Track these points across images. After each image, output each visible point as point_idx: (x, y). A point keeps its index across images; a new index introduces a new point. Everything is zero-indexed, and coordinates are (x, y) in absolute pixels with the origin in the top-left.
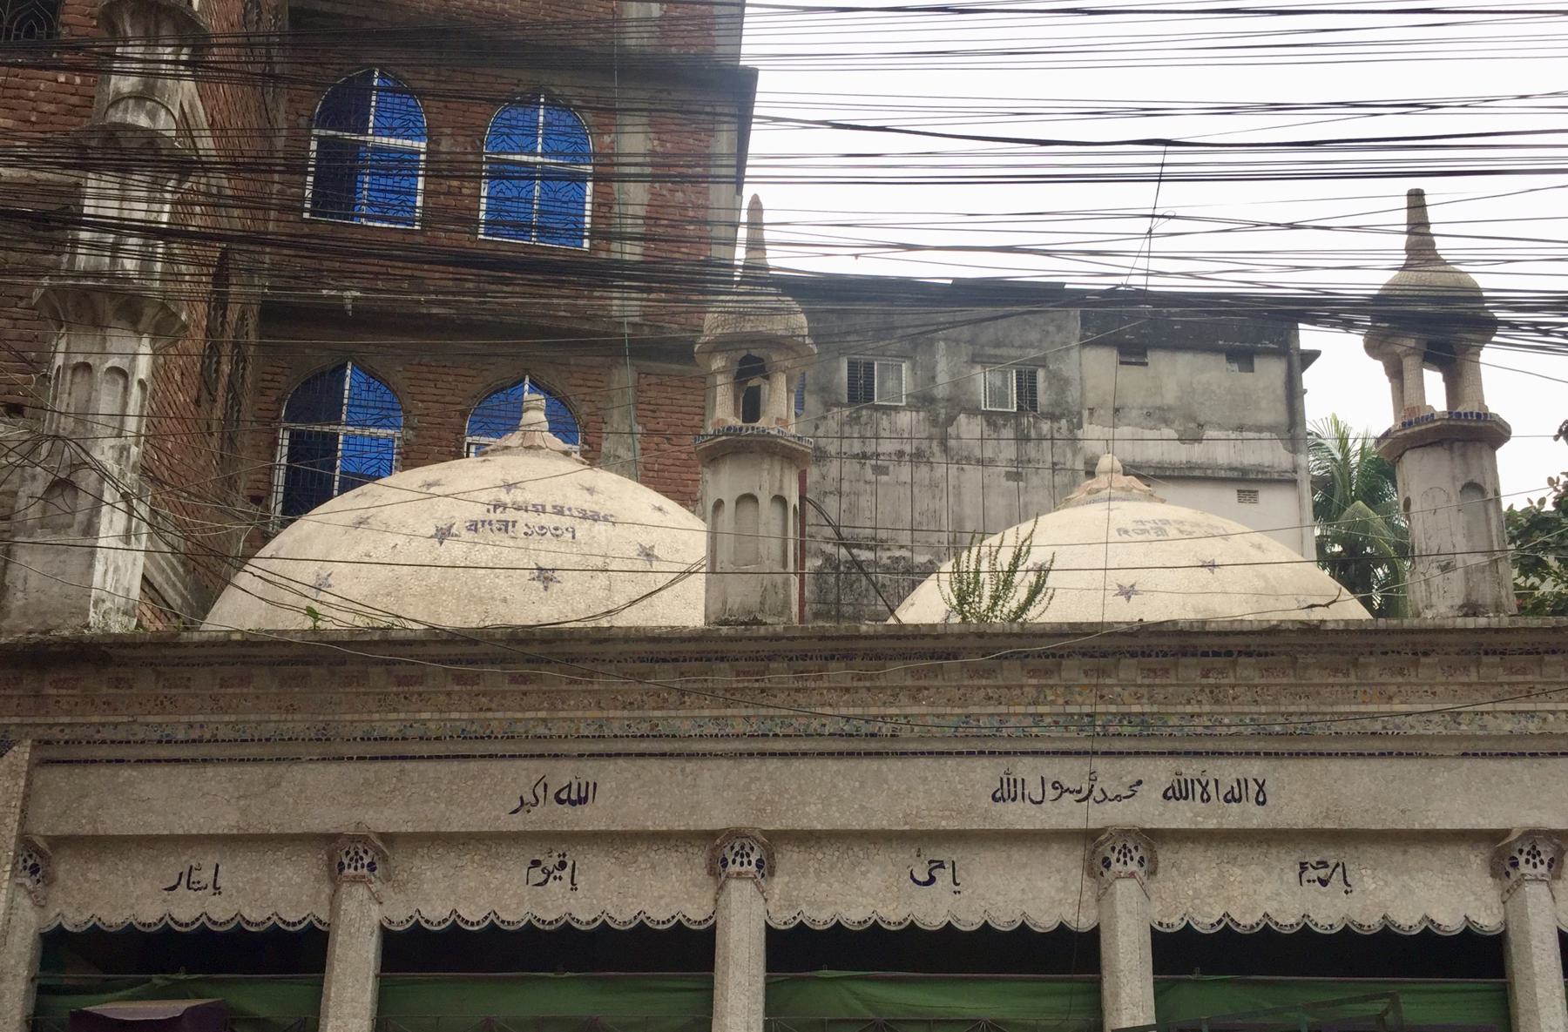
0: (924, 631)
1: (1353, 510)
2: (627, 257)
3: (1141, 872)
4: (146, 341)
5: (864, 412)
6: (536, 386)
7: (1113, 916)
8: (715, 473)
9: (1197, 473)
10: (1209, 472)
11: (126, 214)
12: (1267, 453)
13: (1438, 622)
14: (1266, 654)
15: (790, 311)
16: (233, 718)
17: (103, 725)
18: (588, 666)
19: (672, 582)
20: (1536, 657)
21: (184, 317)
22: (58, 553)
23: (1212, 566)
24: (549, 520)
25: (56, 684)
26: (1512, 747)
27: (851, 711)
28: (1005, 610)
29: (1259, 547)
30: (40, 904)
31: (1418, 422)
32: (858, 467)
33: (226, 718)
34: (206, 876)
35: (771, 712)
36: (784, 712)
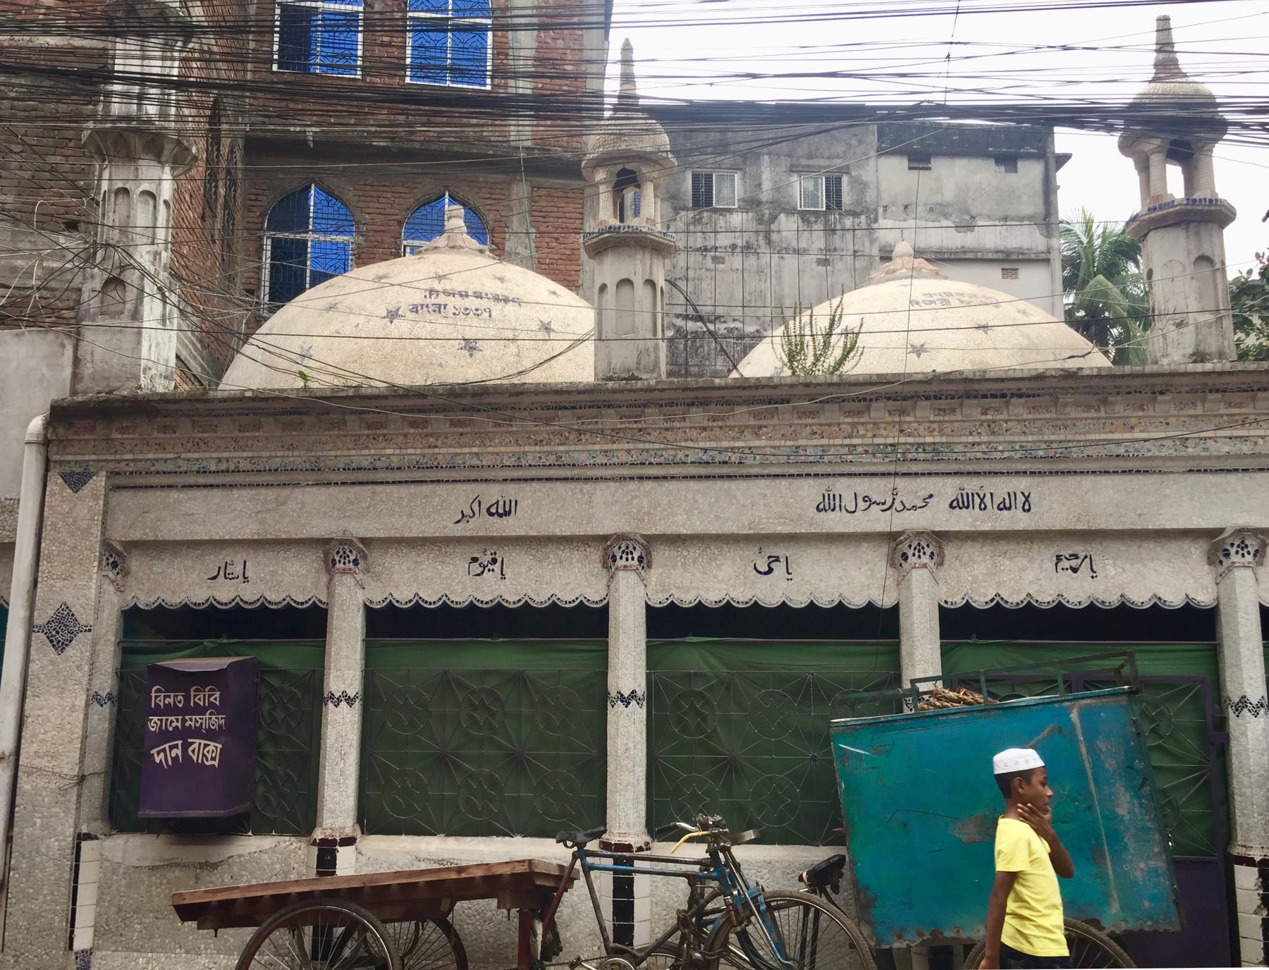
0: (764, 382)
1: (1097, 283)
2: (521, 91)
3: (931, 564)
4: (167, 169)
5: (705, 214)
6: (454, 199)
7: (910, 598)
8: (600, 262)
9: (969, 256)
10: (979, 255)
11: (146, 70)
12: (1026, 238)
13: (1173, 368)
14: (1034, 396)
15: (655, 132)
16: (250, 454)
17: (157, 460)
18: (509, 412)
19: (570, 348)
20: (1250, 394)
21: (194, 150)
22: (114, 334)
23: (985, 327)
24: (471, 303)
25: (122, 430)
26: (1229, 464)
27: (708, 445)
28: (826, 365)
29: (1024, 313)
30: (120, 590)
31: (1161, 208)
32: (700, 258)
33: (245, 454)
34: (238, 569)
35: (647, 446)
36: (657, 446)
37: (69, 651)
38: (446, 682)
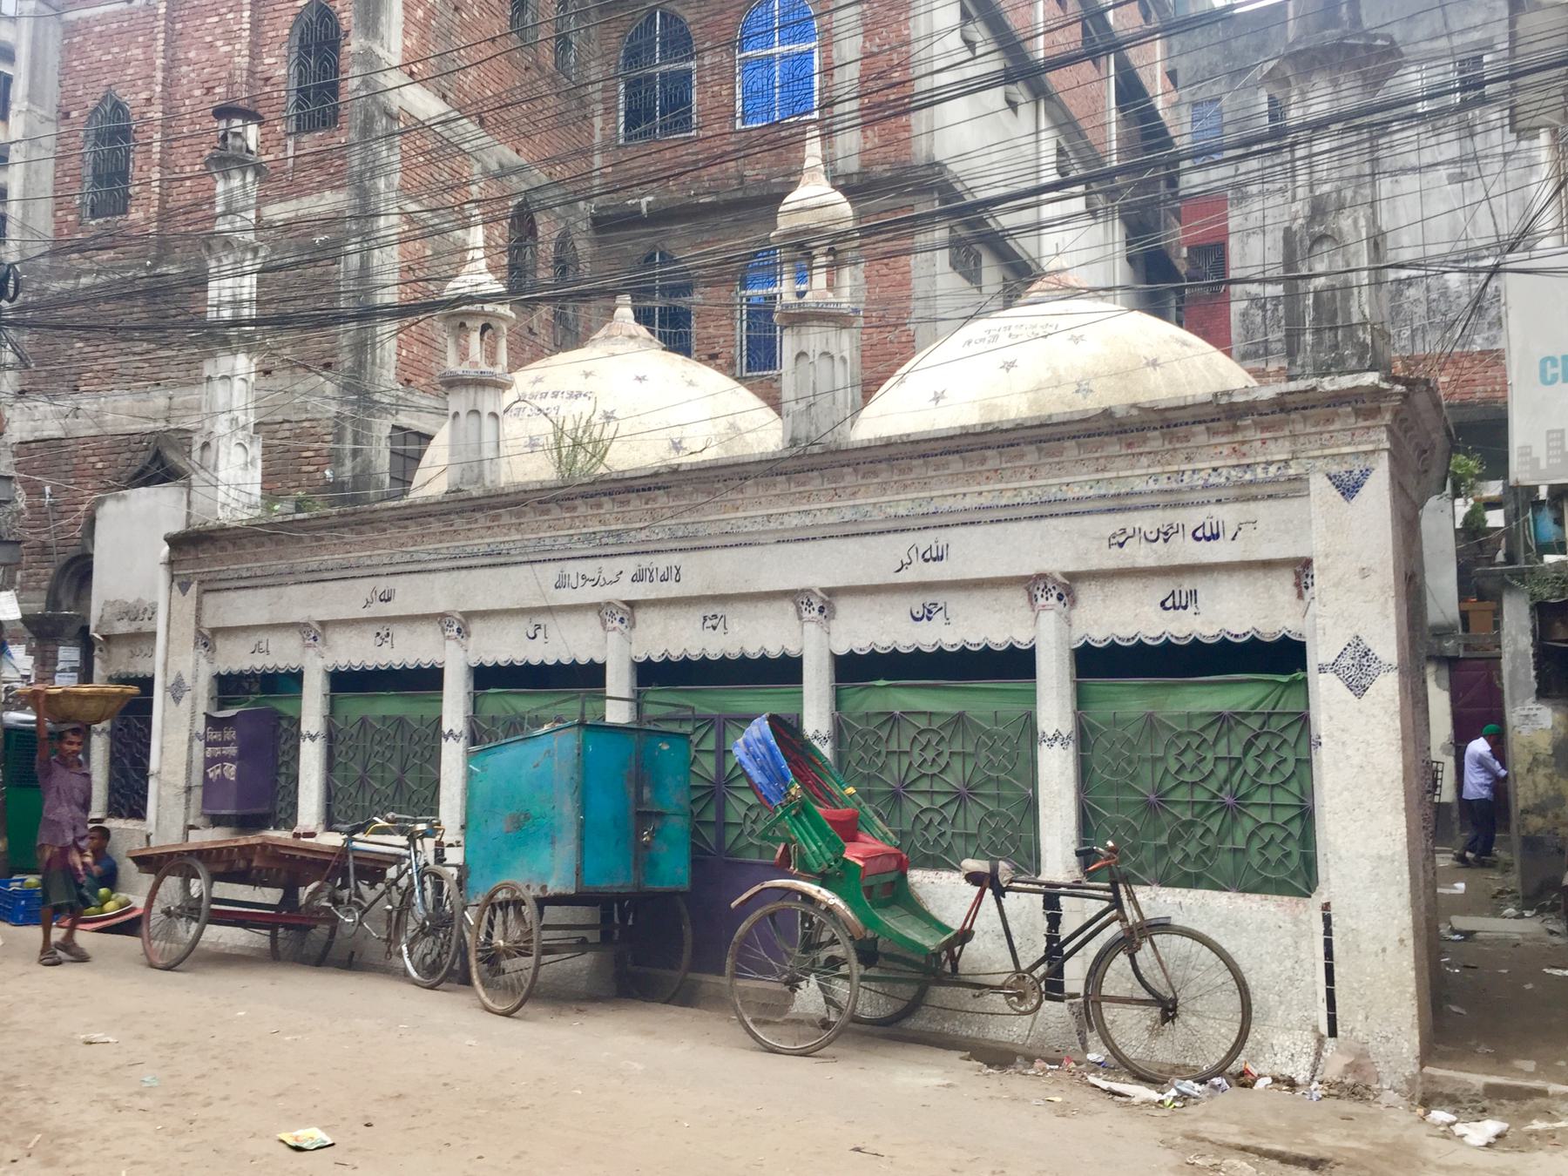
25: (203, 551)
37: (182, 704)
38: (1151, 724)
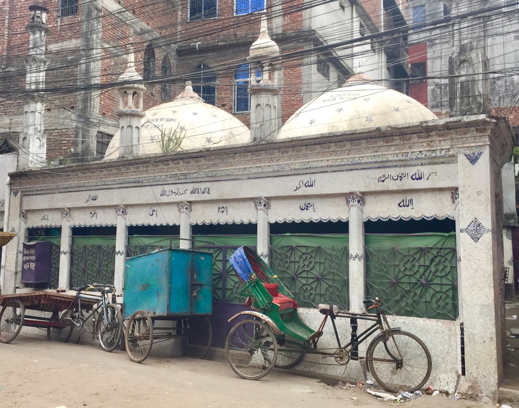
30: (26, 223)
